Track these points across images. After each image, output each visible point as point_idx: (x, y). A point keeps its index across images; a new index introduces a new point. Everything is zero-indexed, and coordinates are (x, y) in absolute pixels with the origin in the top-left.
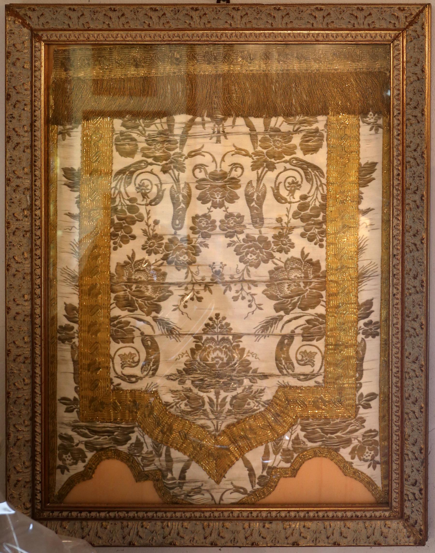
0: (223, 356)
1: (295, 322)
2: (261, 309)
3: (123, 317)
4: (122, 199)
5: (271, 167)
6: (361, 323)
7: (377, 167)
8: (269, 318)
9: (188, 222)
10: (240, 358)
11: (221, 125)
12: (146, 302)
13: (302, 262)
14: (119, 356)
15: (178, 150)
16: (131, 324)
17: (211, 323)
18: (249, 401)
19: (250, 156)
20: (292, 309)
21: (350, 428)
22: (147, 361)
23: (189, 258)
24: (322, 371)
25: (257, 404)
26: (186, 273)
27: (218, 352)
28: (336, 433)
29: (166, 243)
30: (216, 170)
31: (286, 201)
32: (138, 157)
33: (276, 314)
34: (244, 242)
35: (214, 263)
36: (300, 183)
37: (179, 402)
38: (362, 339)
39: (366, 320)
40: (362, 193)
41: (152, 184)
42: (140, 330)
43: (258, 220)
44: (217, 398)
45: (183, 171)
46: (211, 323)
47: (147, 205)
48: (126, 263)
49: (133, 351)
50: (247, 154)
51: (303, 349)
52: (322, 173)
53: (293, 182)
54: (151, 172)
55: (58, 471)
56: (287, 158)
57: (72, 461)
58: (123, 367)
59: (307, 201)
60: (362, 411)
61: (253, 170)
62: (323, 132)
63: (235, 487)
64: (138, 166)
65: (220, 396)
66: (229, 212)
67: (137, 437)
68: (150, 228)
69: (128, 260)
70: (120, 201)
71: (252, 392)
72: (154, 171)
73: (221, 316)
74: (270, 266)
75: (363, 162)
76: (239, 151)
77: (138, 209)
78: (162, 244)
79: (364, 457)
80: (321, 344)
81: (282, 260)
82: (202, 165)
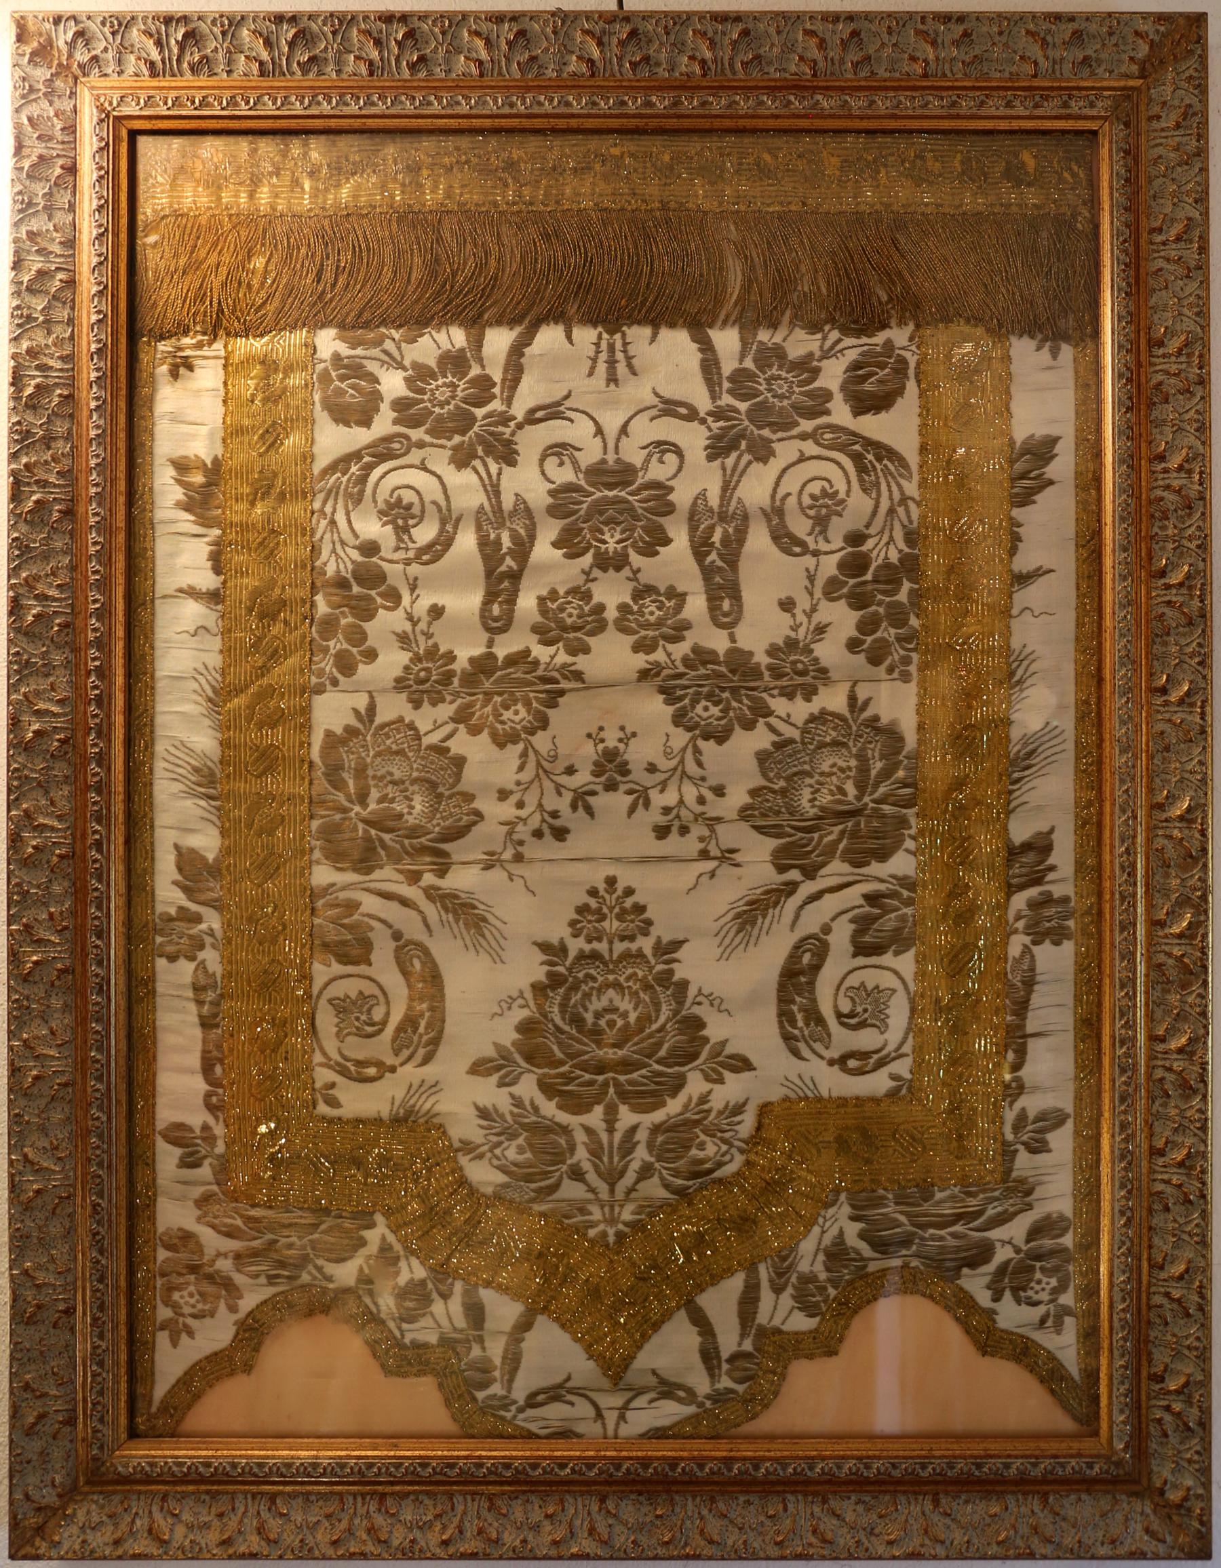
0: (625, 1004)
1: (831, 904)
3: (343, 889)
4: (338, 547)
5: (763, 453)
6: (1019, 901)
7: (1053, 470)
8: (758, 891)
10: (676, 1012)
11: (618, 336)
12: (406, 842)
13: (850, 727)
14: (330, 1001)
15: (496, 405)
16: (363, 909)
17: (593, 903)
19: (703, 421)
21: (990, 1212)
22: (410, 1022)
23: (529, 712)
24: (907, 1048)
25: (724, 1148)
26: (521, 756)
28: (953, 1223)
30: (604, 461)
31: (806, 550)
32: (384, 423)
34: (686, 666)
36: (842, 495)
37: (501, 1143)
38: (1025, 946)
39: (1033, 892)
40: (1020, 525)
42: (390, 927)
44: (611, 1130)
45: (512, 463)
46: (593, 903)
48: (351, 731)
50: (692, 415)
52: (906, 466)
55: (163, 1338)
56: (807, 425)
59: (864, 548)
60: (1023, 1160)
61: (710, 458)
62: (907, 355)
64: (383, 451)
65: (618, 1125)
66: (642, 581)
67: (384, 1238)
68: (418, 629)
69: (353, 722)
70: (334, 551)
71: (709, 1111)
73: (620, 887)
74: (761, 739)
75: (1020, 434)
79: (1030, 1293)
80: (906, 963)
81: (792, 720)
82: (564, 446)
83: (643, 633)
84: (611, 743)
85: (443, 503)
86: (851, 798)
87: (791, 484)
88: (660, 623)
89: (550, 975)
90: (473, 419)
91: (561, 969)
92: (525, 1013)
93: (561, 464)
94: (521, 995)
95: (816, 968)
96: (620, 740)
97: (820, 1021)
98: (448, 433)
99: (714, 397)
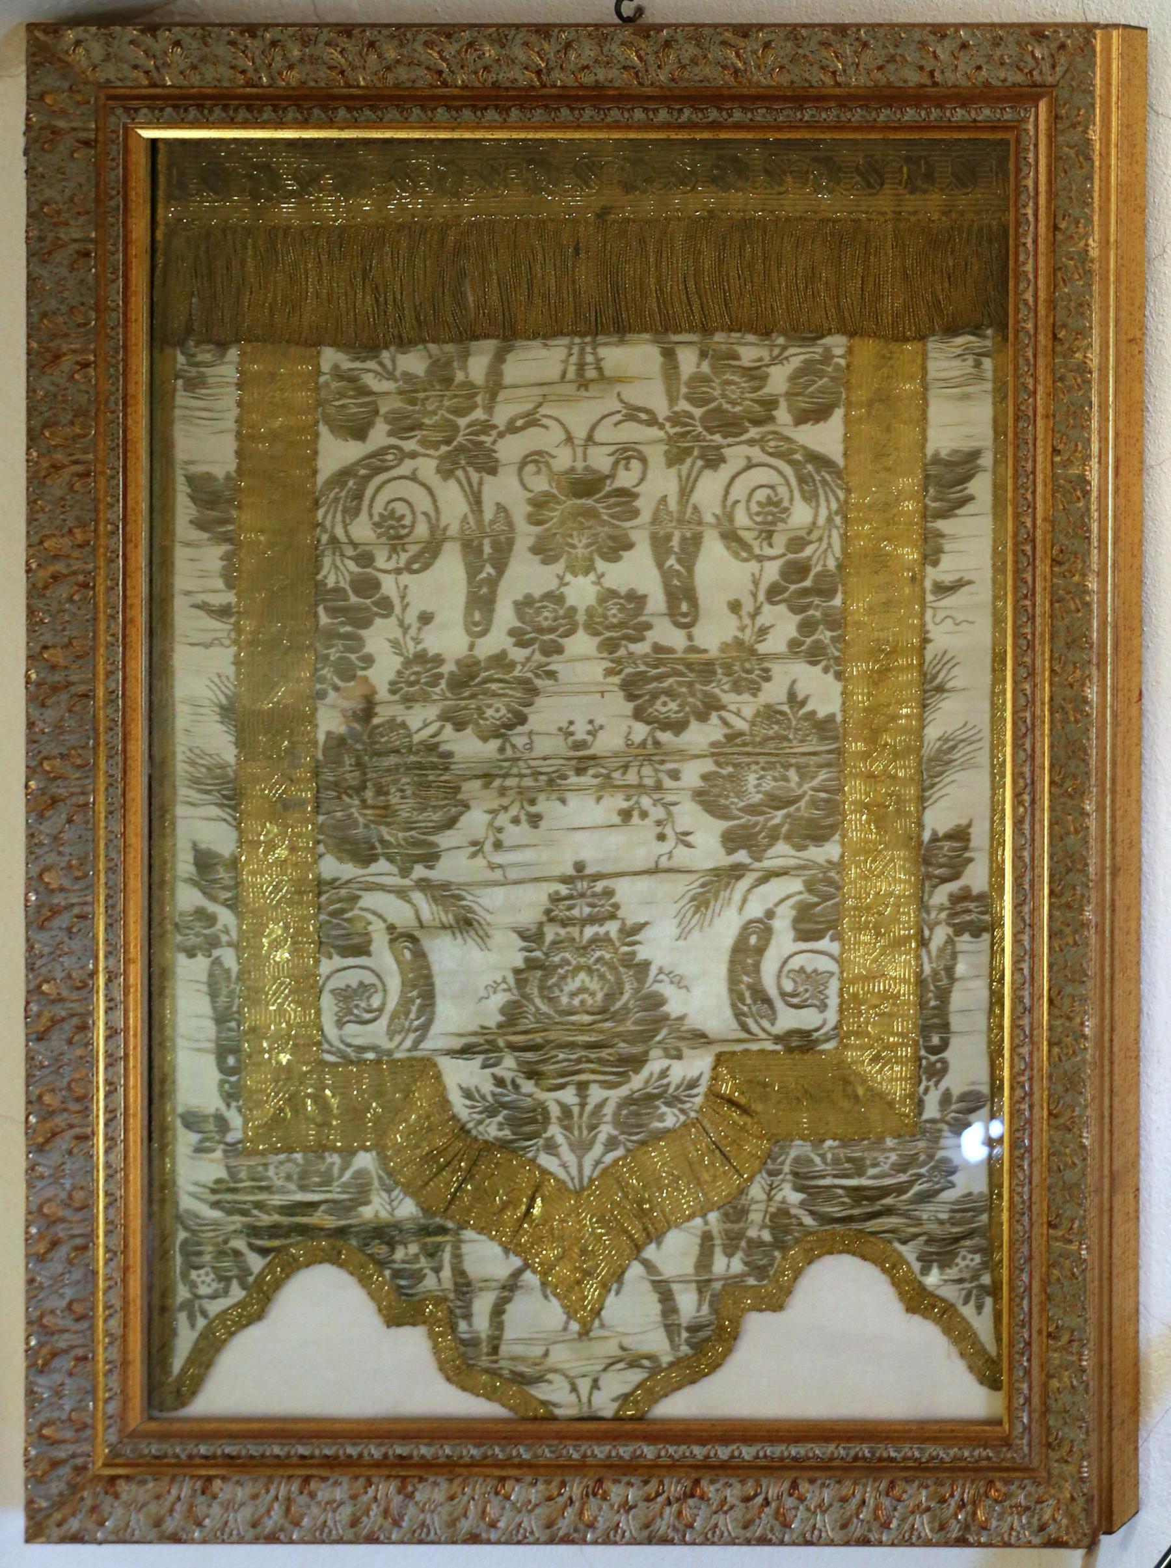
0: (594, 985)
2: (689, 845)
5: (714, 460)
9: (505, 616)
10: (637, 991)
14: (332, 991)
15: (479, 414)
18: (664, 1109)
19: (662, 427)
20: (770, 845)
27: (582, 975)
29: (451, 673)
32: (379, 435)
33: (726, 860)
35: (571, 723)
36: (786, 504)
39: (953, 887)
41: (413, 513)
43: (683, 599)
44: (583, 1105)
45: (493, 471)
47: (398, 571)
49: (369, 978)
50: (653, 422)
51: (795, 963)
53: (770, 502)
54: (413, 478)
55: (182, 1317)
56: (753, 432)
57: (215, 1285)
58: (340, 1024)
63: (627, 405)
64: (376, 463)
72: (421, 475)
76: (633, 413)
77: (377, 585)
78: (440, 676)
82: (539, 453)
83: (608, 634)
84: (580, 735)
85: (432, 513)
86: (793, 785)
87: (739, 491)
88: (622, 625)
89: (527, 960)
90: (456, 428)
91: (538, 954)
92: (507, 997)
93: (538, 472)
94: (504, 980)
95: (760, 951)
96: (589, 733)
97: (767, 1001)
98: (435, 445)
99: (672, 399)
